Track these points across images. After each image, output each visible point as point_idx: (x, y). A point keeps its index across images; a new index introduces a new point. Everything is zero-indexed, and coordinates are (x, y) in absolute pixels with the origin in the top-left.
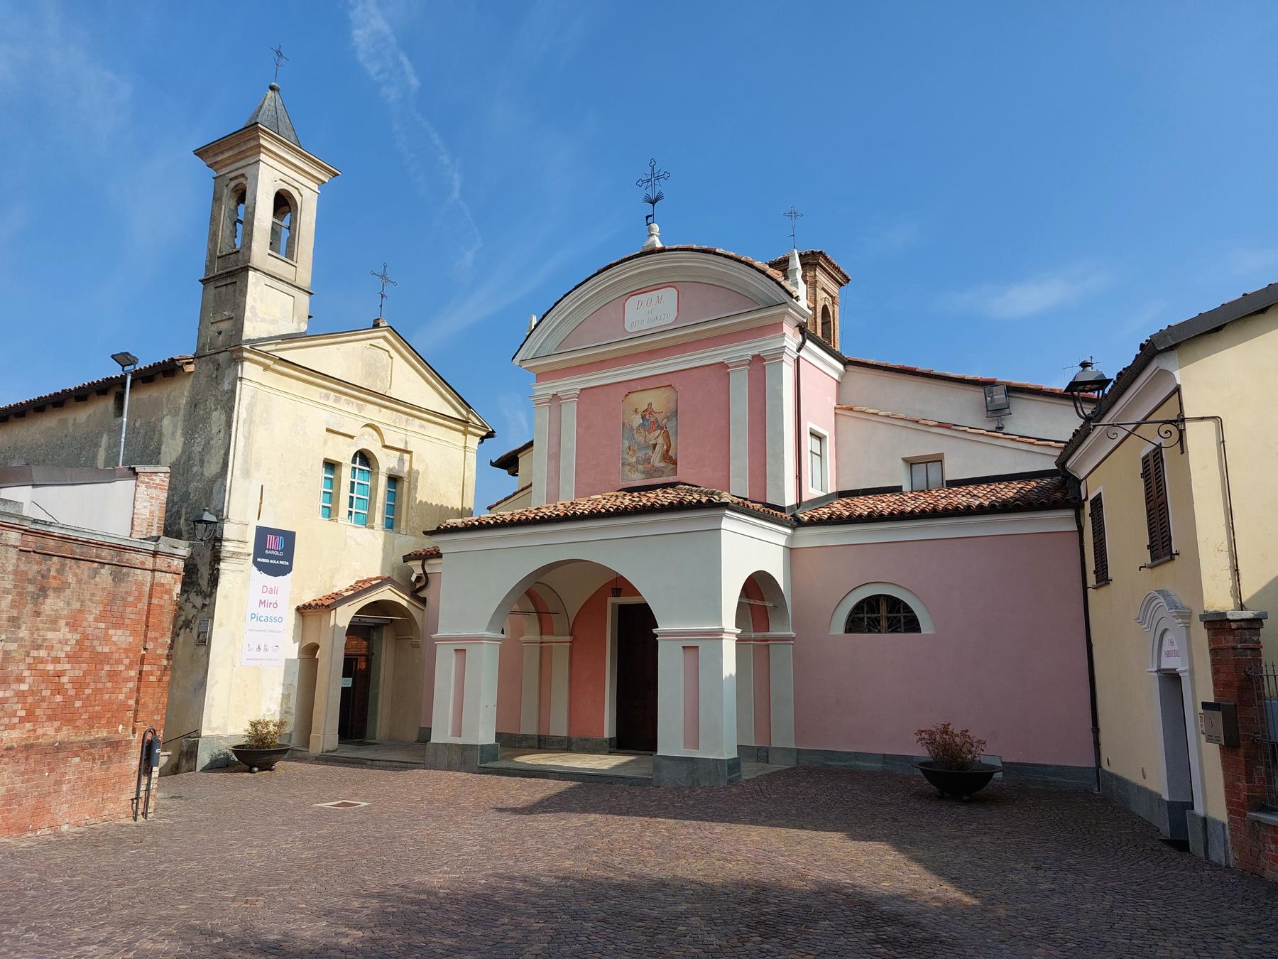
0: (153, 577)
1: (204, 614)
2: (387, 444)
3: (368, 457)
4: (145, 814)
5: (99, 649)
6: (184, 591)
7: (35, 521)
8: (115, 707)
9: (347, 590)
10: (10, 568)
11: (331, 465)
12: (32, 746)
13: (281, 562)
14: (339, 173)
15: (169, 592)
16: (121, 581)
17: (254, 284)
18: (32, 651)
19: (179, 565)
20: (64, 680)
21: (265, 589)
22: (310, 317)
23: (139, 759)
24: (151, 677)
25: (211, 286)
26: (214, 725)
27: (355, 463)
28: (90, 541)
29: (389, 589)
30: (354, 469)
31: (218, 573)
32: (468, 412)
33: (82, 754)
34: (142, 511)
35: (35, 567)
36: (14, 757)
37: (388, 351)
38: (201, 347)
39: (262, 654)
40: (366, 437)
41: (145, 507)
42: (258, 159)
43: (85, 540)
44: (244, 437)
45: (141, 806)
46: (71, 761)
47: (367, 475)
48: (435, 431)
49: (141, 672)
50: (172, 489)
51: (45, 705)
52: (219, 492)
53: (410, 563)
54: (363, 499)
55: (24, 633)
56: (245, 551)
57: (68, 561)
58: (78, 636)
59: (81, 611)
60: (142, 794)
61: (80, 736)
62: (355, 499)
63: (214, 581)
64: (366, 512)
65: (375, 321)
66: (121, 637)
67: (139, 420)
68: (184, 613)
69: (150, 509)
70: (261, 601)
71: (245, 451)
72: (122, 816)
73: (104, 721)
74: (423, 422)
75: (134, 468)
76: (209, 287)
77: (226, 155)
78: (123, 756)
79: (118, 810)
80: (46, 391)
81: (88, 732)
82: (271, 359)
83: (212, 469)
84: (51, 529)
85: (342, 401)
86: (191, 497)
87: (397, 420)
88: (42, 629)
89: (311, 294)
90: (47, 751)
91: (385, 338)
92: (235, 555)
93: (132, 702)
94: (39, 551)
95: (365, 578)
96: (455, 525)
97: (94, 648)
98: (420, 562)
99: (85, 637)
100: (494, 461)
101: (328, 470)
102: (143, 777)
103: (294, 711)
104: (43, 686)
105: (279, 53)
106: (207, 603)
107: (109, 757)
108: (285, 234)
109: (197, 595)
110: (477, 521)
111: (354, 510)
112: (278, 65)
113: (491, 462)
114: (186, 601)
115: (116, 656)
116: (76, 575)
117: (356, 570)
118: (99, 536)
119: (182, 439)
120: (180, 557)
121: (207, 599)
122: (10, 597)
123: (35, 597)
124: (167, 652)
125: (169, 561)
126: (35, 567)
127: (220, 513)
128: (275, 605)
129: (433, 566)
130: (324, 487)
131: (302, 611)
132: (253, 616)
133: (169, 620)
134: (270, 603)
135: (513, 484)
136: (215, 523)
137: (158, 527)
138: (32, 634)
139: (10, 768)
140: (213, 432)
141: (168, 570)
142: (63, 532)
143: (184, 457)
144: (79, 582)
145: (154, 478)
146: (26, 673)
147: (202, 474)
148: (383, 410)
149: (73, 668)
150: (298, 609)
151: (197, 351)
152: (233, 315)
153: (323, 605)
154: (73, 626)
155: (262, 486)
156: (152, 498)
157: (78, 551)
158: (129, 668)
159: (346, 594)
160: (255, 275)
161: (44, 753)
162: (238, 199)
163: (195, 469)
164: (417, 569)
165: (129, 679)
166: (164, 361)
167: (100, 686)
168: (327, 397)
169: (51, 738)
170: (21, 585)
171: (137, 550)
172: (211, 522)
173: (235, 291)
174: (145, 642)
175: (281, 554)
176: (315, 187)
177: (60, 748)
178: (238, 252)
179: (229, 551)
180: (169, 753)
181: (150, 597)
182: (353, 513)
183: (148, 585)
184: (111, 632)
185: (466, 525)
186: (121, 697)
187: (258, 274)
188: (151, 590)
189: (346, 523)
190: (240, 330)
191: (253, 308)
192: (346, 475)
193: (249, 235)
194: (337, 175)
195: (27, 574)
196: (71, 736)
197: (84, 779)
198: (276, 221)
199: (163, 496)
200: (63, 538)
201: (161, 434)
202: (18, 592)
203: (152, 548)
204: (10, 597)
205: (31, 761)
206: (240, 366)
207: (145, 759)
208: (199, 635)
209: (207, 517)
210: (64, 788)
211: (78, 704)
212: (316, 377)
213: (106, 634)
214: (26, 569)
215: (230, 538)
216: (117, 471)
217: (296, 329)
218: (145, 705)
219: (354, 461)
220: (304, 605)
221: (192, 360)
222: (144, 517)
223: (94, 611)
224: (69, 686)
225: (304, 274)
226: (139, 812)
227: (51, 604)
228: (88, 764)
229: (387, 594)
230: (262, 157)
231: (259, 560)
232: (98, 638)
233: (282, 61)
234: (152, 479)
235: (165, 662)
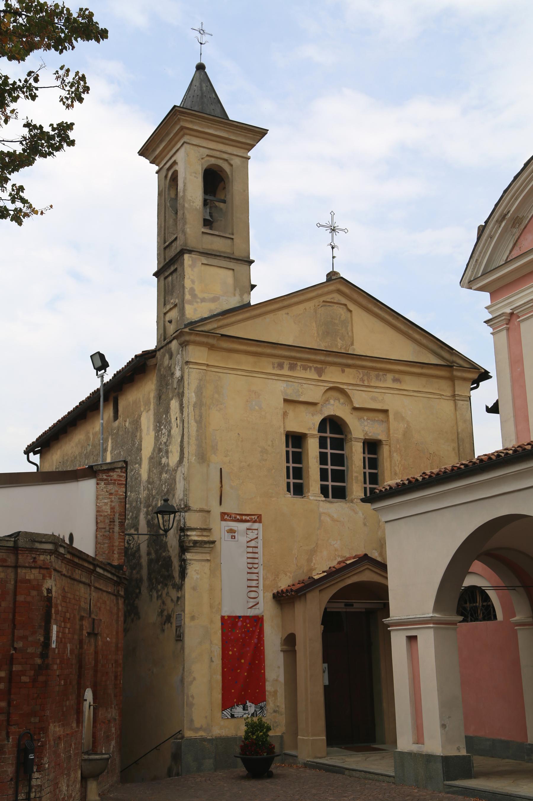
0: (16, 574)
17: (190, 266)
26: (197, 725)
29: (368, 568)
37: (345, 305)
40: (332, 402)
41: (106, 504)
44: (196, 422)
63: (183, 574)
67: (128, 420)
69: (111, 505)
85: (298, 368)
103: (283, 710)
105: (202, 32)
112: (201, 44)
113: (487, 407)
117: (336, 550)
119: (154, 433)
124: (39, 650)
125: (33, 556)
137: (119, 522)
145: (111, 474)
156: (111, 494)
160: (191, 257)
174: (13, 641)
183: (13, 582)
189: (319, 499)
198: (208, 197)
208: (176, 630)
215: (193, 526)
217: (239, 302)
222: (106, 514)
235: (38, 661)
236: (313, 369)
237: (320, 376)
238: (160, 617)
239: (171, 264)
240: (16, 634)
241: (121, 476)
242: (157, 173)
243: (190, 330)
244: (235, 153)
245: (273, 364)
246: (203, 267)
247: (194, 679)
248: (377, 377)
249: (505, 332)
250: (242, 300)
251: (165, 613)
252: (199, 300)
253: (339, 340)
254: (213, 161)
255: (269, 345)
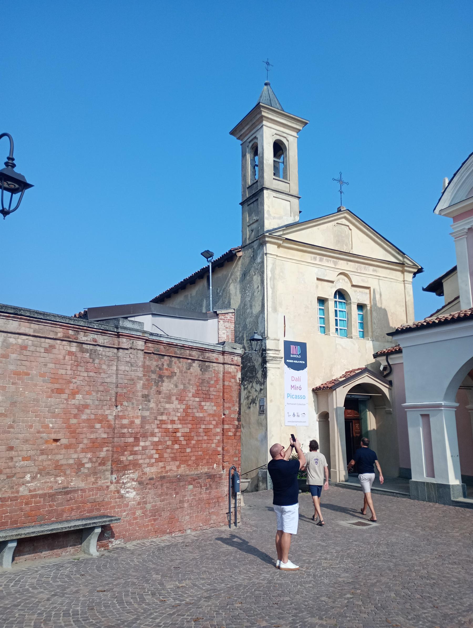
0: (224, 368)
1: (262, 395)
2: (354, 284)
3: (343, 293)
4: (235, 523)
5: (197, 415)
6: (243, 379)
7: (152, 334)
8: (210, 452)
9: (341, 377)
10: (140, 364)
11: (322, 301)
12: (164, 477)
13: (300, 362)
14: (308, 122)
15: (234, 377)
16: (206, 370)
18: (158, 416)
19: (238, 360)
20: (179, 434)
21: (293, 379)
22: (300, 212)
23: (228, 487)
24: (229, 433)
25: (246, 205)
27: (336, 298)
28: (185, 345)
29: (367, 376)
30: (336, 302)
31: (266, 369)
32: (404, 257)
33: (194, 483)
34: (223, 336)
35: (155, 363)
36: (154, 484)
37: (348, 226)
38: (244, 241)
39: (296, 418)
40: (341, 281)
41: (224, 333)
42: (262, 125)
43: (182, 345)
44: (271, 288)
45: (233, 518)
46: (188, 487)
47: (344, 305)
48: (382, 272)
49: (223, 429)
50: (237, 323)
51: (169, 451)
52: (261, 323)
53: (379, 359)
54: (343, 320)
55: (152, 405)
56: (279, 356)
57: (173, 359)
58: (184, 407)
59: (184, 390)
60: (232, 510)
61: (192, 471)
62: (338, 320)
63: (265, 375)
64: (346, 328)
65: (338, 209)
66: (209, 407)
67: (219, 289)
68: (251, 394)
70: (291, 386)
71: (272, 296)
72: (222, 524)
73: (205, 461)
74: (375, 268)
75: (216, 312)
76: (244, 207)
77: (246, 128)
78: (218, 484)
79: (219, 520)
80: (177, 281)
81: (196, 469)
82: (281, 240)
83: (256, 310)
84: (161, 339)
85: (324, 260)
86: (248, 327)
87: (359, 268)
88: (163, 403)
89: (299, 198)
90: (174, 481)
91: (345, 218)
92: (274, 358)
93: (220, 449)
94: (156, 352)
95: (351, 370)
96: (408, 327)
97: (194, 414)
98: (384, 358)
99: (188, 407)
100: (425, 287)
101: (320, 304)
102: (231, 499)
104: (167, 438)
105: (268, 63)
106: (262, 388)
107: (210, 485)
108: (281, 166)
109: (257, 384)
110: (425, 322)
111: (339, 327)
114: (252, 387)
115: (207, 419)
116: (179, 367)
117: (345, 365)
118: (190, 343)
119: (240, 295)
120: (238, 355)
121: (262, 386)
122: (142, 382)
123: (157, 382)
125: (232, 357)
126: (155, 363)
127: (264, 334)
128: (300, 388)
129: (394, 360)
130: (320, 315)
131: (316, 391)
132: (289, 395)
133: (236, 395)
134: (297, 387)
135: (441, 301)
136: (261, 340)
138: (157, 405)
139: (152, 492)
140: (255, 288)
141: (232, 363)
142: (168, 340)
143: (242, 305)
144: (181, 372)
145: (227, 316)
146: (156, 430)
147: (252, 313)
148: (349, 263)
149: (183, 428)
150: (313, 390)
151: (242, 243)
152: (258, 218)
153: (327, 387)
154: (181, 400)
155: (284, 316)
156: (227, 328)
157: (178, 352)
158: (216, 426)
159: (341, 380)
161: (171, 482)
162: (254, 154)
163: (248, 311)
164: (383, 362)
165: (216, 435)
166: (227, 253)
167: (200, 438)
168: (315, 259)
169: (175, 472)
170: (148, 374)
171: (213, 351)
172: (259, 340)
173: (258, 204)
174: (224, 410)
175: (300, 357)
176: (295, 134)
177: (180, 479)
178: (257, 181)
179: (271, 356)
180: (249, 480)
181: (224, 381)
182: (339, 330)
183: (222, 373)
184: (203, 404)
185: (417, 326)
186: (213, 445)
187: (269, 191)
188: (224, 376)
190: (263, 225)
191: (268, 211)
192: (331, 304)
193: (262, 170)
194: (306, 123)
195: (150, 367)
196: (187, 471)
197: (197, 499)
198: (276, 159)
199: (232, 326)
200: (169, 344)
201: (230, 294)
202: (146, 379)
203: (221, 349)
204: (142, 382)
205: (164, 487)
206: (265, 247)
207: (232, 487)
209: (257, 337)
210: (186, 505)
211: (188, 450)
212: (308, 247)
213: (200, 405)
214: (149, 364)
215: (270, 348)
216: (208, 314)
218: (228, 451)
219: (335, 297)
220: (317, 388)
221: (240, 250)
223: (192, 390)
224: (182, 439)
225: (294, 187)
226: (232, 522)
227: (167, 386)
228: (198, 490)
229: (366, 379)
230: (264, 123)
231: (288, 361)
232: (196, 408)
233: (270, 67)
234: (226, 317)
235: (236, 423)
236: (332, 261)
237: (335, 265)
238: (247, 400)
239: (254, 197)
240: (225, 406)
241: (232, 318)
242: (241, 145)
243: (269, 234)
244: (290, 134)
245: (311, 257)
246: (274, 198)
247: (273, 435)
248: (365, 268)
249: (465, 239)
250: (295, 219)
251: (251, 398)
252: (272, 218)
253: (344, 246)
254: (278, 138)
255: (310, 246)
